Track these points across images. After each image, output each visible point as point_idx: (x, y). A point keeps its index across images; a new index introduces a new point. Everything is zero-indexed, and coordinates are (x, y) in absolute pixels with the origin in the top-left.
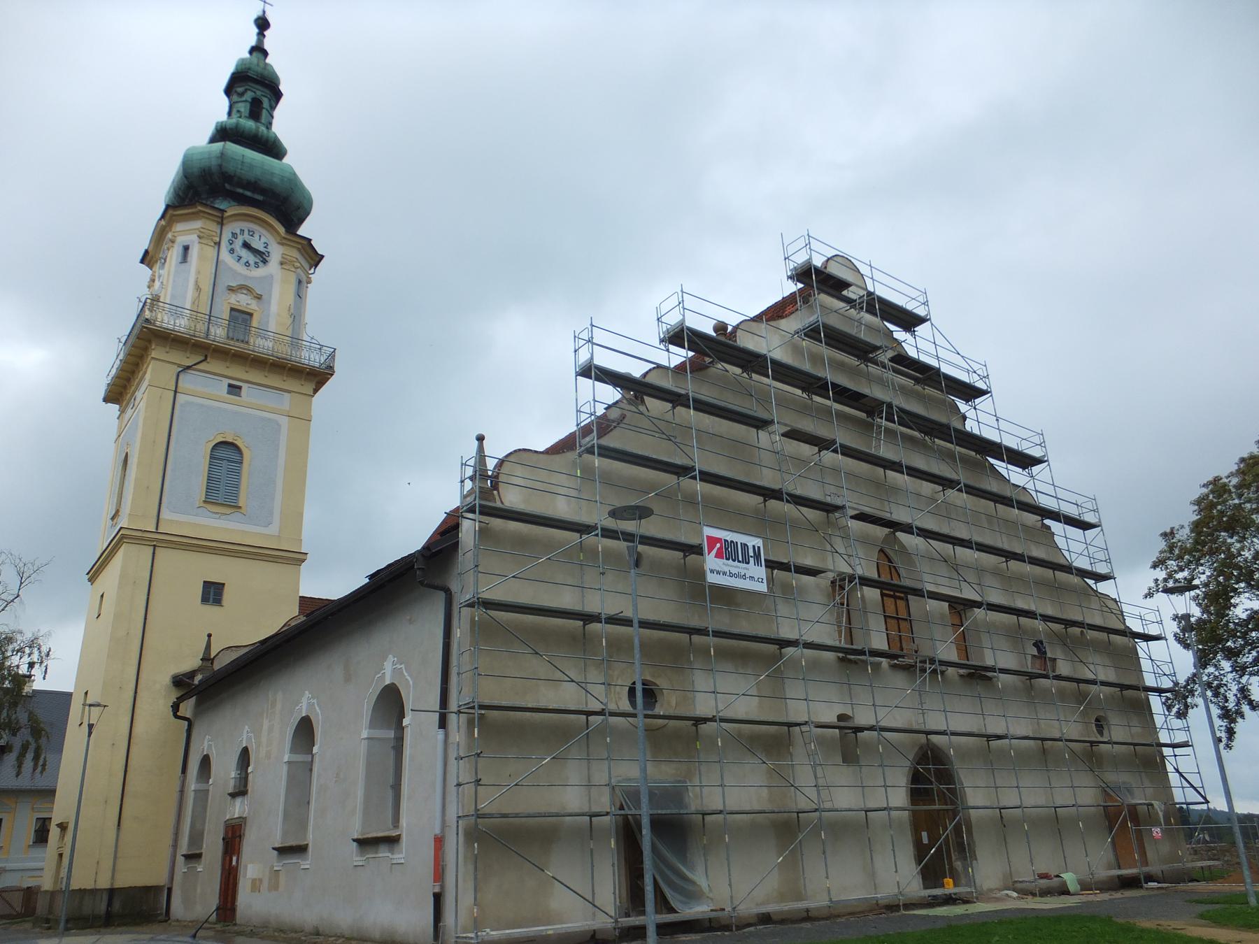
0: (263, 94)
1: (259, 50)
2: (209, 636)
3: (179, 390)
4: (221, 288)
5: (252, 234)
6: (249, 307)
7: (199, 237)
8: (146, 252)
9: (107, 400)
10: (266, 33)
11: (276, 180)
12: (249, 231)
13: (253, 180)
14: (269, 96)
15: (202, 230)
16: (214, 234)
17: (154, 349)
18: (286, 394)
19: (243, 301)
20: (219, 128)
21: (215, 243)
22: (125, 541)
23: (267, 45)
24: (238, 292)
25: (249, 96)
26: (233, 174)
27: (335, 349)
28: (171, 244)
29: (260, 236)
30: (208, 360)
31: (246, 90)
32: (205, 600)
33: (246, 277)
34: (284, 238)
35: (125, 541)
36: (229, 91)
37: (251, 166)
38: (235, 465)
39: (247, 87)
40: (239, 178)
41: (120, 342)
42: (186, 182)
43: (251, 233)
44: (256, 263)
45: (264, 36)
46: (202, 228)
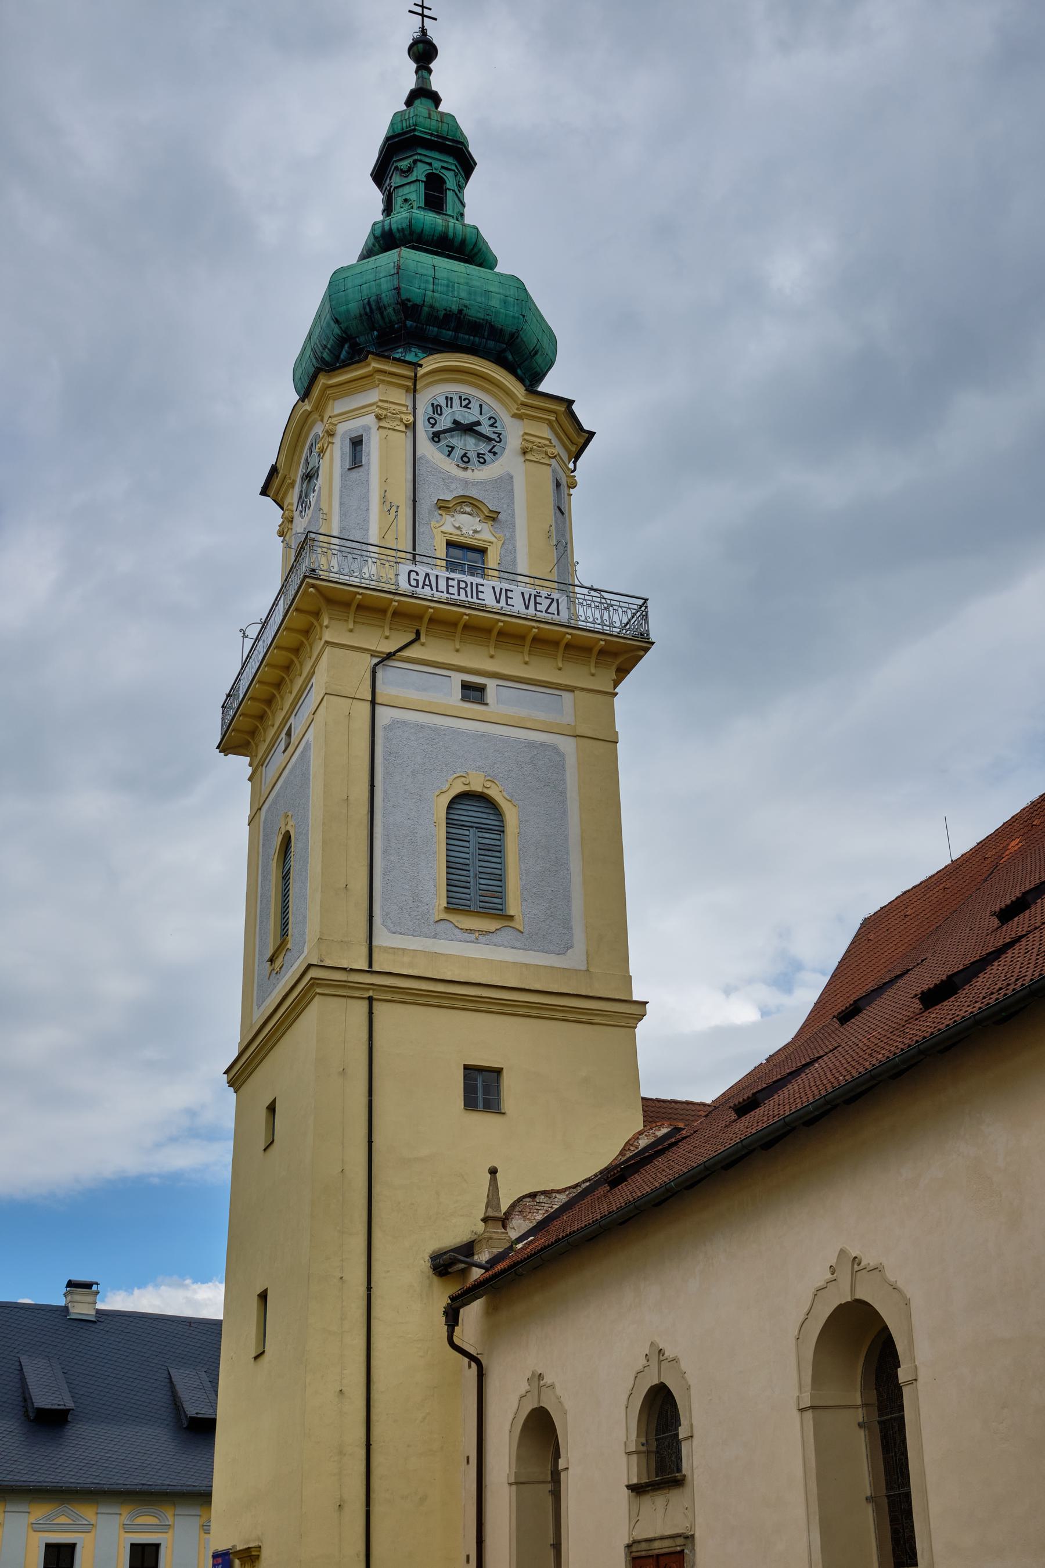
0: (445, 165)
1: (423, 31)
2: (493, 1172)
3: (378, 700)
4: (426, 504)
5: (466, 402)
6: (477, 536)
7: (379, 418)
8: (274, 470)
9: (226, 747)
10: (432, 66)
11: (495, 302)
12: (460, 398)
13: (455, 308)
14: (454, 168)
15: (380, 404)
16: (404, 409)
17: (327, 627)
18: (566, 695)
20: (378, 233)
21: (406, 426)
22: (318, 990)
23: (437, 83)
25: (420, 172)
26: (419, 301)
27: (646, 600)
28: (328, 439)
29: (481, 406)
30: (423, 639)
31: (415, 162)
32: (470, 1103)
33: (466, 482)
34: (524, 404)
35: (318, 990)
36: (379, 176)
37: (450, 285)
38: (492, 836)
39: (416, 157)
40: (431, 307)
41: (245, 636)
42: (337, 331)
43: (464, 403)
45: (430, 71)
46: (381, 401)
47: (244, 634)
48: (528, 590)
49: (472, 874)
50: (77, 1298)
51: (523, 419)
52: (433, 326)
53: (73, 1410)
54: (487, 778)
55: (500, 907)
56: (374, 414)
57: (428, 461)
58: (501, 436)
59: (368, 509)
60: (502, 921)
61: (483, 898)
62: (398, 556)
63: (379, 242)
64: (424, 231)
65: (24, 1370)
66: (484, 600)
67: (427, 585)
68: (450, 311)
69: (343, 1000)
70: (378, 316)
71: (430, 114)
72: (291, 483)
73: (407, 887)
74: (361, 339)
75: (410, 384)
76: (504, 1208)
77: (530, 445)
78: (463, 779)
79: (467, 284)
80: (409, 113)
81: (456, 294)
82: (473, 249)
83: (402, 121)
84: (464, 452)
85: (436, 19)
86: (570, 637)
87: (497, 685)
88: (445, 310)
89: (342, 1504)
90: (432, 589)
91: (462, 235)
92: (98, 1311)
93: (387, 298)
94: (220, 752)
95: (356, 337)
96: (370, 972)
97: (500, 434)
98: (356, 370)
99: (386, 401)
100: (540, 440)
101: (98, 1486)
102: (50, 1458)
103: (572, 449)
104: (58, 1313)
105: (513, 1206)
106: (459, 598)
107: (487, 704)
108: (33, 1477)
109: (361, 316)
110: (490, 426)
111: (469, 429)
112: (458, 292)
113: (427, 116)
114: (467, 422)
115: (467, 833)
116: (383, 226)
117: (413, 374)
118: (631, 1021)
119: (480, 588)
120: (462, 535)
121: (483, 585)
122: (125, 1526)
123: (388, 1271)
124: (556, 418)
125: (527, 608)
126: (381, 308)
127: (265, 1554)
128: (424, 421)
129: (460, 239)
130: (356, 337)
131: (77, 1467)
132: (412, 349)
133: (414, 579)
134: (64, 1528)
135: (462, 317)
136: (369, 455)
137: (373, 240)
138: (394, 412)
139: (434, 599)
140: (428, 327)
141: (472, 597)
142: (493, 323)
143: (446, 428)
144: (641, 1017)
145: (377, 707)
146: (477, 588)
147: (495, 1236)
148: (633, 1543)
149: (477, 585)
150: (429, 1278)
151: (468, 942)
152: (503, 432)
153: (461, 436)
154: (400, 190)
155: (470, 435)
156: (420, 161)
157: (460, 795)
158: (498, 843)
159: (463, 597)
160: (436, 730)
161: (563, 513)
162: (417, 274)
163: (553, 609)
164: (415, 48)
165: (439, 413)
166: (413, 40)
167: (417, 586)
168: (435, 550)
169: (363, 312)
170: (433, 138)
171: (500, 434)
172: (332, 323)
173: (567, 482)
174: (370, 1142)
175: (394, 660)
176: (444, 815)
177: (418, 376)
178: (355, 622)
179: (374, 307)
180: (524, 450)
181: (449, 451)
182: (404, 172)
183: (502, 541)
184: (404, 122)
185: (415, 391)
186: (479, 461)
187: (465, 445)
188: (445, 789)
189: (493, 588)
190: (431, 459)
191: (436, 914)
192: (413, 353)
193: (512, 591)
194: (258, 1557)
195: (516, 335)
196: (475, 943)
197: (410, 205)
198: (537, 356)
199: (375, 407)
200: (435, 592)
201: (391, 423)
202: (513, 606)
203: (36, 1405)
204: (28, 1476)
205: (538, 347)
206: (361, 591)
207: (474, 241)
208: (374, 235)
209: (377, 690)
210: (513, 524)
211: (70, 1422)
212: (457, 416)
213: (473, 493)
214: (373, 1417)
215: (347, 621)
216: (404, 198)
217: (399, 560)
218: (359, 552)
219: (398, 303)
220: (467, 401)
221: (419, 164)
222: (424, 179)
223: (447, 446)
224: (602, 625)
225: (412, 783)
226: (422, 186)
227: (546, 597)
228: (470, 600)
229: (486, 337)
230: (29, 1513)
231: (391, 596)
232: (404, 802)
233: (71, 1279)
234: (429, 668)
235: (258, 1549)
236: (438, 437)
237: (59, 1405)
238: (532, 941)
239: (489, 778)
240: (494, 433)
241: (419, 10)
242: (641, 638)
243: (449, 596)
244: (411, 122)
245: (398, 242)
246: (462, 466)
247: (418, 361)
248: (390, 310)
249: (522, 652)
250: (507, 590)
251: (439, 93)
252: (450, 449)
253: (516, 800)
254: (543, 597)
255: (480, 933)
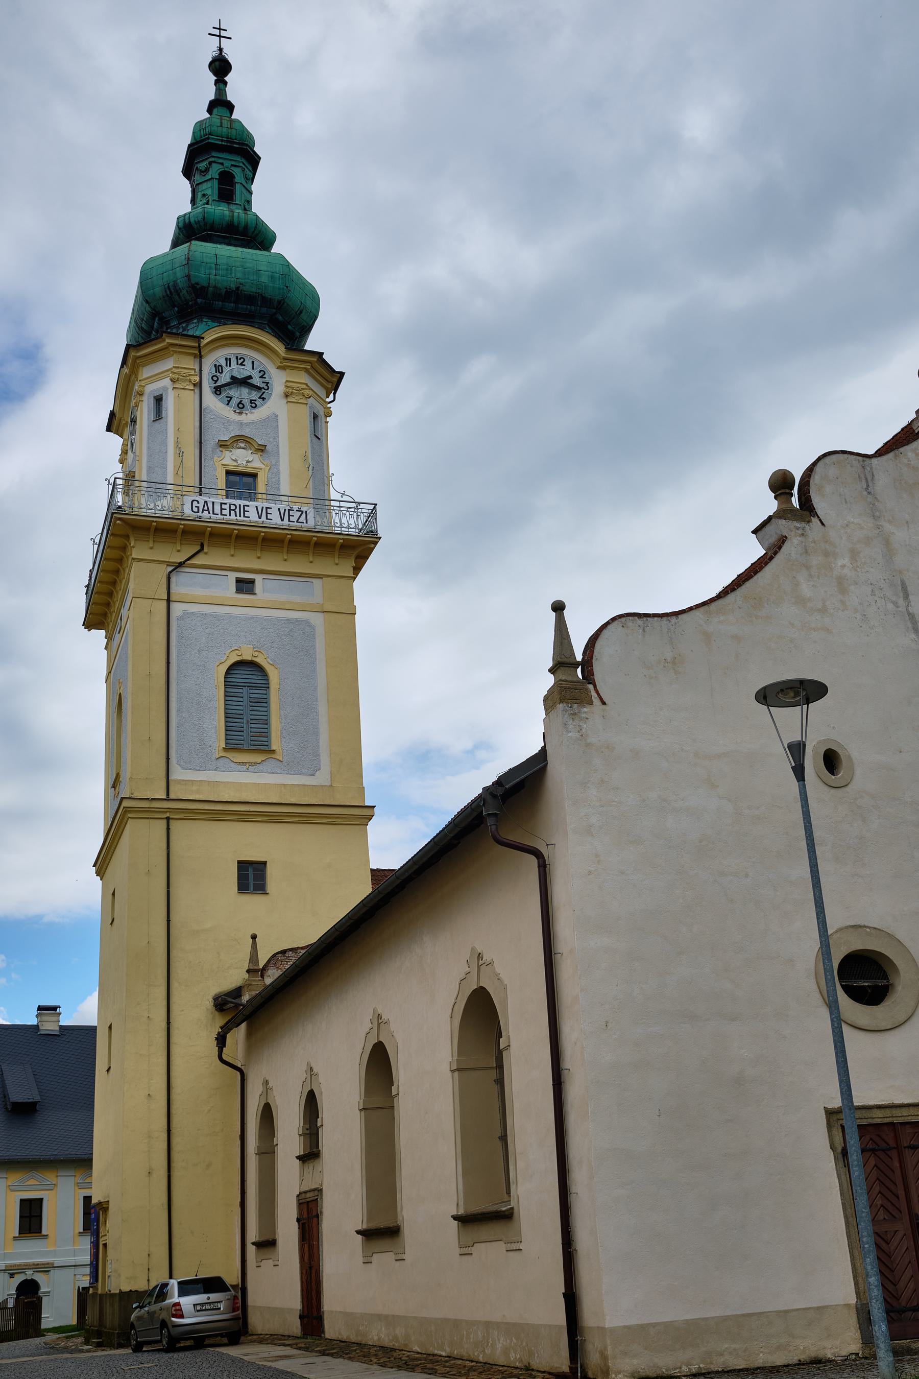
0: (234, 163)
1: (221, 50)
2: (254, 937)
4: (209, 445)
5: (241, 361)
6: (249, 465)
11: (264, 279)
12: (237, 357)
13: (233, 286)
14: (241, 164)
17: (133, 547)
19: (241, 458)
20: (181, 225)
21: (194, 385)
22: (130, 815)
24: (233, 447)
26: (205, 284)
27: (376, 505)
29: (253, 362)
30: (206, 550)
31: (210, 163)
33: (241, 424)
34: (285, 359)
35: (130, 815)
36: (188, 171)
37: (229, 269)
39: (211, 160)
40: (215, 287)
42: (148, 309)
43: (240, 362)
44: (251, 402)
45: (225, 83)
47: (94, 542)
48: (282, 507)
49: (245, 721)
50: (45, 1018)
51: (286, 370)
52: (218, 301)
53: (39, 1102)
54: (255, 650)
55: (266, 743)
56: (169, 378)
57: (211, 411)
58: (269, 385)
59: (166, 452)
60: (267, 755)
61: (253, 738)
62: (184, 490)
63: (182, 232)
64: (215, 222)
65: (4, 1075)
66: (249, 517)
67: (205, 510)
68: (230, 289)
69: (147, 821)
70: (176, 297)
71: (221, 123)
72: (125, 424)
73: (195, 735)
74: (166, 314)
75: (197, 352)
76: (261, 965)
77: (291, 390)
78: (237, 651)
79: (242, 266)
80: (206, 123)
81: (233, 275)
82: (254, 231)
83: (200, 130)
84: (240, 400)
85: (230, 38)
86: (316, 539)
87: (264, 579)
88: (226, 288)
89: (150, 1171)
90: (209, 513)
91: (245, 222)
92: (61, 1027)
93: (182, 283)
94: (85, 628)
95: (162, 313)
96: (168, 800)
97: (268, 383)
98: (156, 344)
99: (178, 367)
100: (299, 385)
101: (57, 1157)
102: (21, 1138)
103: (328, 386)
104: (32, 1030)
105: (269, 961)
106: (230, 517)
107: (255, 594)
108: (8, 1153)
109: (164, 297)
110: (260, 377)
111: (245, 382)
112: (235, 274)
113: (219, 124)
114: (242, 376)
115: (241, 691)
116: (184, 219)
117: (197, 345)
118: (363, 820)
119: (246, 508)
120: (238, 466)
121: (248, 506)
122: (79, 1184)
123: (182, 1010)
124: (312, 366)
125: (282, 520)
126: (178, 292)
127: (111, 1206)
128: (208, 379)
129: (243, 225)
130: (162, 313)
131: (42, 1144)
132: (204, 320)
133: (196, 507)
134: (34, 1188)
135: (239, 292)
136: (167, 410)
137: (178, 230)
138: (185, 375)
139: (211, 520)
140: (214, 302)
141: (240, 516)
142: (263, 295)
143: (226, 382)
144: (370, 817)
145: (171, 604)
146: (244, 508)
147: (253, 983)
148: (299, 1194)
149: (244, 506)
150: (212, 1013)
151: (241, 772)
152: (270, 382)
153: (238, 387)
154: (200, 186)
155: (245, 387)
156: (215, 162)
157: (236, 663)
158: (265, 696)
159: (233, 517)
160: (216, 616)
161: (319, 439)
162: (202, 263)
163: (303, 519)
164: (213, 65)
165: (220, 371)
166: (212, 58)
167: (198, 512)
168: (217, 479)
169: (164, 294)
170: (223, 143)
171: (268, 383)
172: (144, 303)
173: (325, 412)
174: (168, 921)
175: (184, 567)
176: (222, 679)
177: (201, 345)
178: (154, 541)
179: (173, 291)
180: (285, 394)
181: (228, 401)
182: (203, 172)
183: (269, 467)
184: (202, 130)
185: (201, 357)
186: (251, 406)
187: (241, 395)
188: (223, 661)
189: (257, 507)
190: (214, 408)
191: (217, 753)
192: (205, 323)
193: (271, 508)
194: (108, 1208)
195: (282, 301)
196: (247, 772)
197: (207, 198)
198: (302, 315)
199: (170, 372)
200: (211, 514)
201: (183, 384)
202: (272, 520)
203: (11, 1100)
204: (4, 1152)
205: (302, 308)
206: (155, 519)
207: (254, 225)
208: (178, 227)
209: (171, 591)
210: (278, 453)
211: (39, 1111)
212: (234, 372)
213: (247, 432)
214: (173, 1111)
215: (148, 541)
216: (203, 193)
217: (184, 493)
218: (153, 490)
219: (189, 287)
220: (242, 360)
221: (214, 165)
222: (218, 177)
223: (227, 397)
224: (341, 528)
225: (199, 658)
226: (216, 182)
227: (297, 511)
228: (238, 518)
229: (260, 305)
230: (6, 1178)
231: (178, 522)
232: (193, 673)
233: (40, 1004)
234: (213, 571)
235: (107, 1203)
236: (220, 391)
237: (29, 1099)
238: (289, 768)
239: (257, 649)
240: (263, 382)
241: (217, 32)
242: (371, 535)
243: (222, 517)
244: (207, 130)
245: (196, 231)
246: (238, 411)
247: (201, 335)
248: (184, 292)
249: (282, 552)
250: (267, 508)
251: (231, 101)
252: (229, 399)
253: (278, 663)
254: (295, 510)
255: (250, 764)
